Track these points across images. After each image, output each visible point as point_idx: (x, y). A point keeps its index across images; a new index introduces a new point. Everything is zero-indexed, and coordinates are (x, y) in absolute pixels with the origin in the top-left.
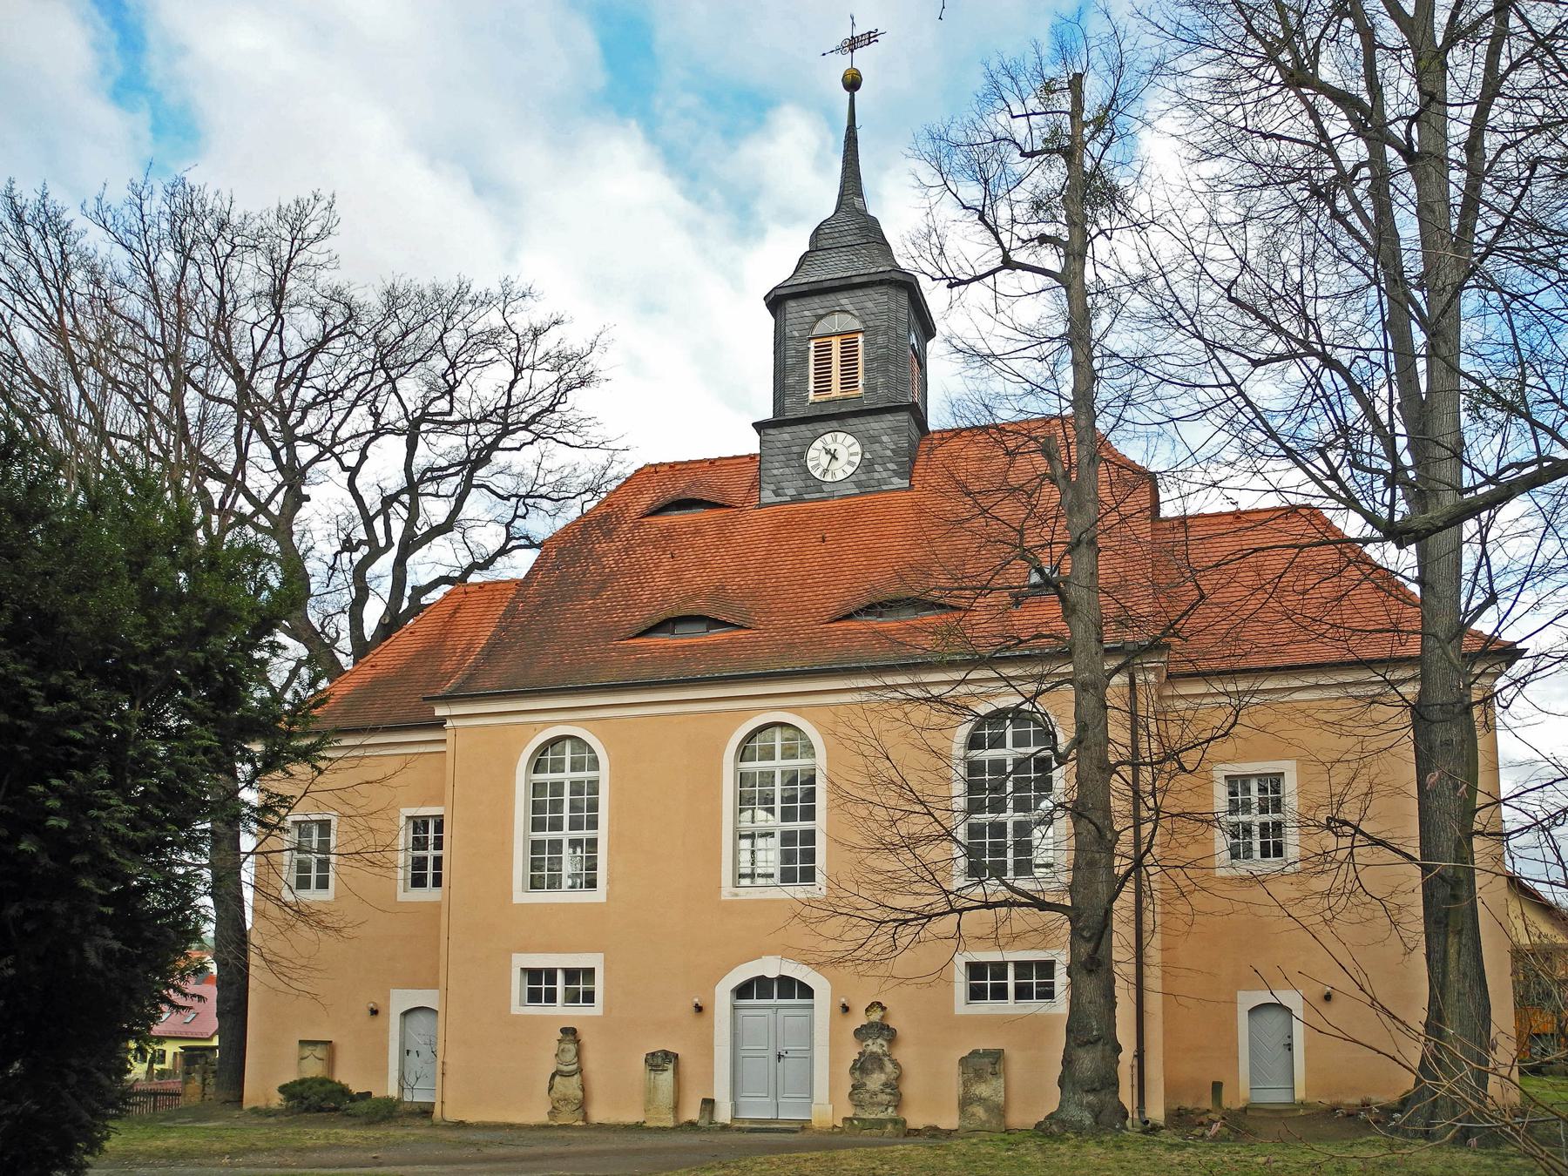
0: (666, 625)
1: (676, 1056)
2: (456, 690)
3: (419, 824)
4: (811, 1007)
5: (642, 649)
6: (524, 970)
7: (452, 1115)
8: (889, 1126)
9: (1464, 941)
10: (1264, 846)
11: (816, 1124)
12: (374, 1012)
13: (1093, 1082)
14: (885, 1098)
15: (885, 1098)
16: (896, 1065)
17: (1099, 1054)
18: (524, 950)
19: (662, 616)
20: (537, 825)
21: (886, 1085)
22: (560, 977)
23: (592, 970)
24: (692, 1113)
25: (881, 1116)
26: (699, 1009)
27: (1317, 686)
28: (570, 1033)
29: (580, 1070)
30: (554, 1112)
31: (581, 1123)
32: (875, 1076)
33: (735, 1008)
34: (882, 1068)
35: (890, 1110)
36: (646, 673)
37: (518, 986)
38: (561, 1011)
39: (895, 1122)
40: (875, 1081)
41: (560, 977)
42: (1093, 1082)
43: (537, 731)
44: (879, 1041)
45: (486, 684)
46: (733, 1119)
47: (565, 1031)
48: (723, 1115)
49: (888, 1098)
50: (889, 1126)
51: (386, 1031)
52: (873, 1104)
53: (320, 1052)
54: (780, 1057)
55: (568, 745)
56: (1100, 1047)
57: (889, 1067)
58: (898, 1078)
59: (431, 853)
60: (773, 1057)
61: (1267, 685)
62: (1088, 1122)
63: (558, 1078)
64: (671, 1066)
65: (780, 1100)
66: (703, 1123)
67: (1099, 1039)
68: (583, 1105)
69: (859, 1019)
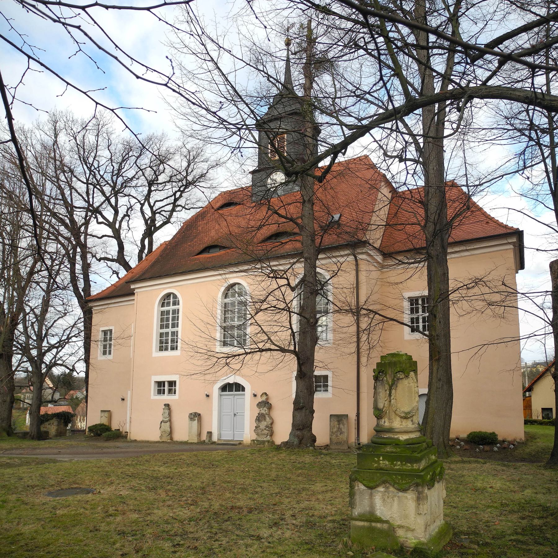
0: (207, 249)
1: (199, 415)
2: (139, 277)
3: (105, 332)
4: (244, 395)
5: (199, 259)
6: (156, 382)
7: (133, 438)
8: (266, 443)
9: (441, 364)
10: (417, 322)
11: (245, 442)
12: (123, 399)
13: (299, 426)
14: (266, 432)
15: (266, 432)
16: (271, 418)
17: (303, 414)
18: (156, 375)
19: (206, 245)
20: (162, 327)
21: (267, 426)
22: (166, 384)
23: (175, 382)
24: (204, 437)
25: (265, 439)
26: (208, 396)
27: (467, 250)
28: (167, 406)
29: (170, 421)
30: (161, 437)
31: (169, 441)
32: (263, 423)
33: (221, 395)
34: (265, 420)
35: (268, 437)
36: (195, 268)
37: (153, 388)
38: (166, 398)
39: (268, 441)
40: (263, 425)
41: (166, 384)
42: (299, 426)
43: (161, 292)
44: (265, 408)
45: (146, 276)
46: (218, 439)
47: (165, 405)
48: (215, 438)
49: (267, 432)
50: (266, 443)
51: (212, 403)
52: (262, 434)
53: (106, 414)
54: (235, 415)
55: (237, 286)
56: (304, 410)
57: (268, 419)
58: (272, 424)
59: (108, 342)
60: (233, 415)
61: (98, 304)
62: (295, 443)
63: (163, 423)
64: (196, 419)
65: (235, 432)
66: (207, 441)
67: (303, 407)
68: (171, 433)
69: (259, 399)
